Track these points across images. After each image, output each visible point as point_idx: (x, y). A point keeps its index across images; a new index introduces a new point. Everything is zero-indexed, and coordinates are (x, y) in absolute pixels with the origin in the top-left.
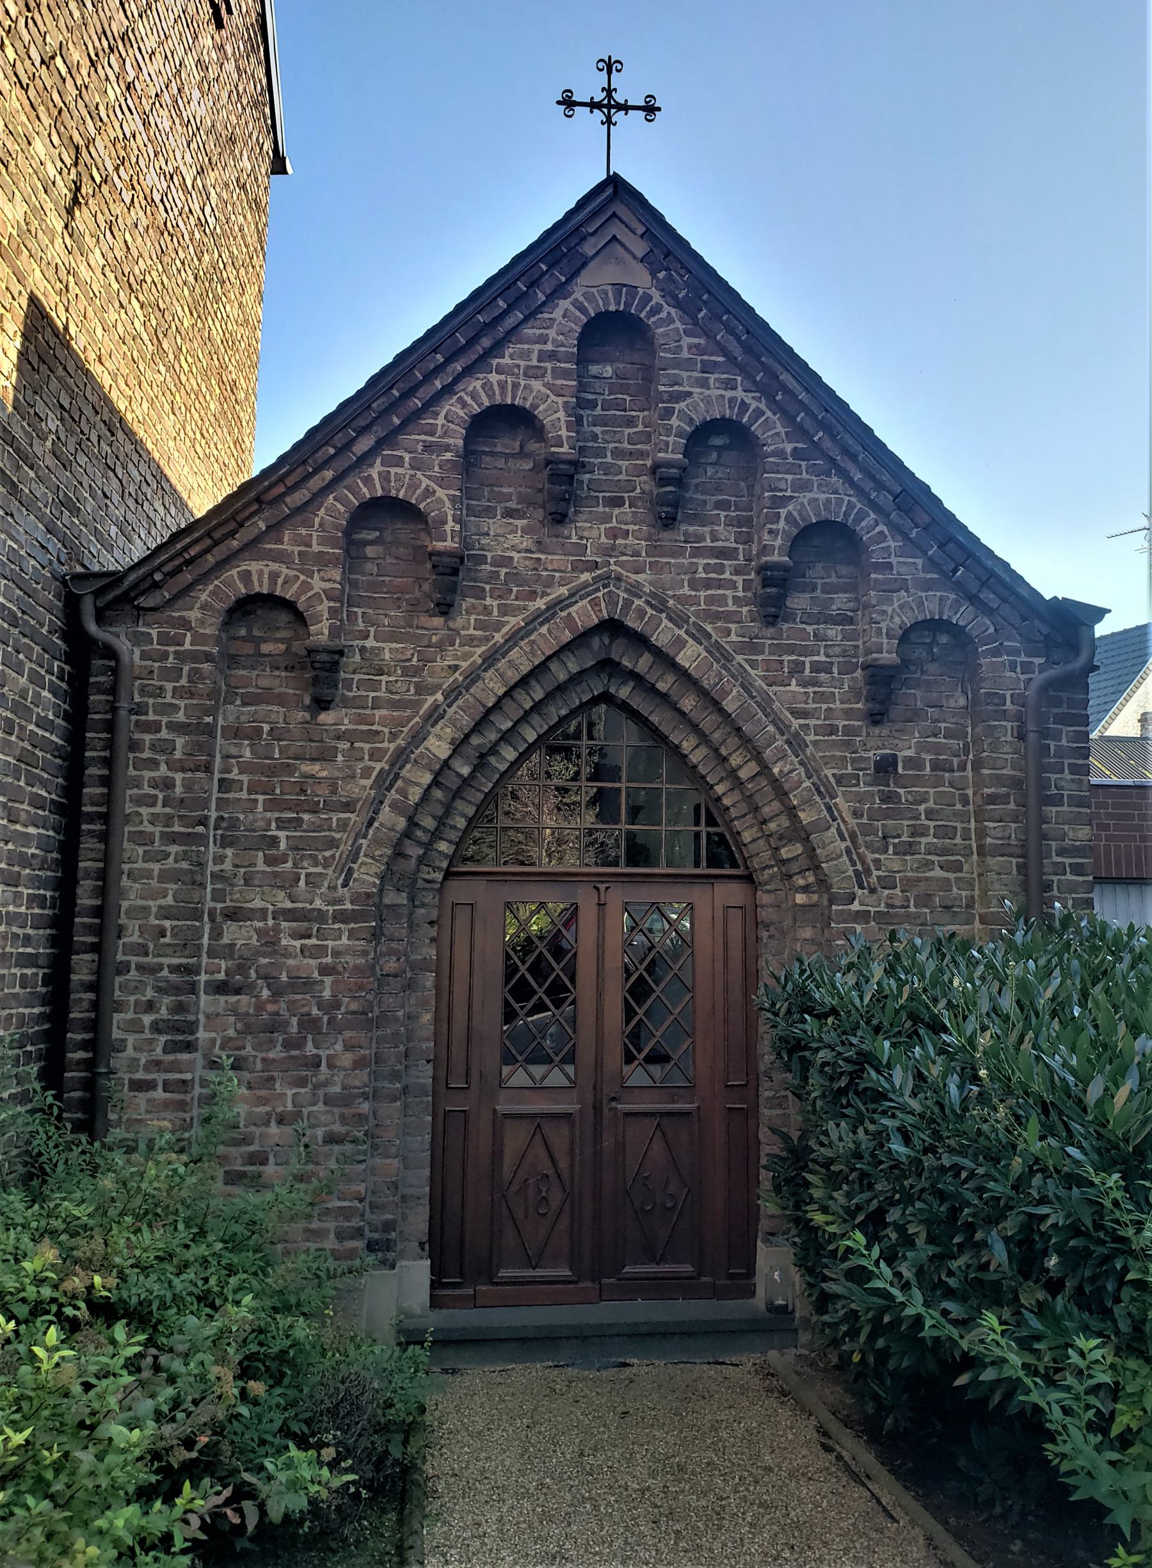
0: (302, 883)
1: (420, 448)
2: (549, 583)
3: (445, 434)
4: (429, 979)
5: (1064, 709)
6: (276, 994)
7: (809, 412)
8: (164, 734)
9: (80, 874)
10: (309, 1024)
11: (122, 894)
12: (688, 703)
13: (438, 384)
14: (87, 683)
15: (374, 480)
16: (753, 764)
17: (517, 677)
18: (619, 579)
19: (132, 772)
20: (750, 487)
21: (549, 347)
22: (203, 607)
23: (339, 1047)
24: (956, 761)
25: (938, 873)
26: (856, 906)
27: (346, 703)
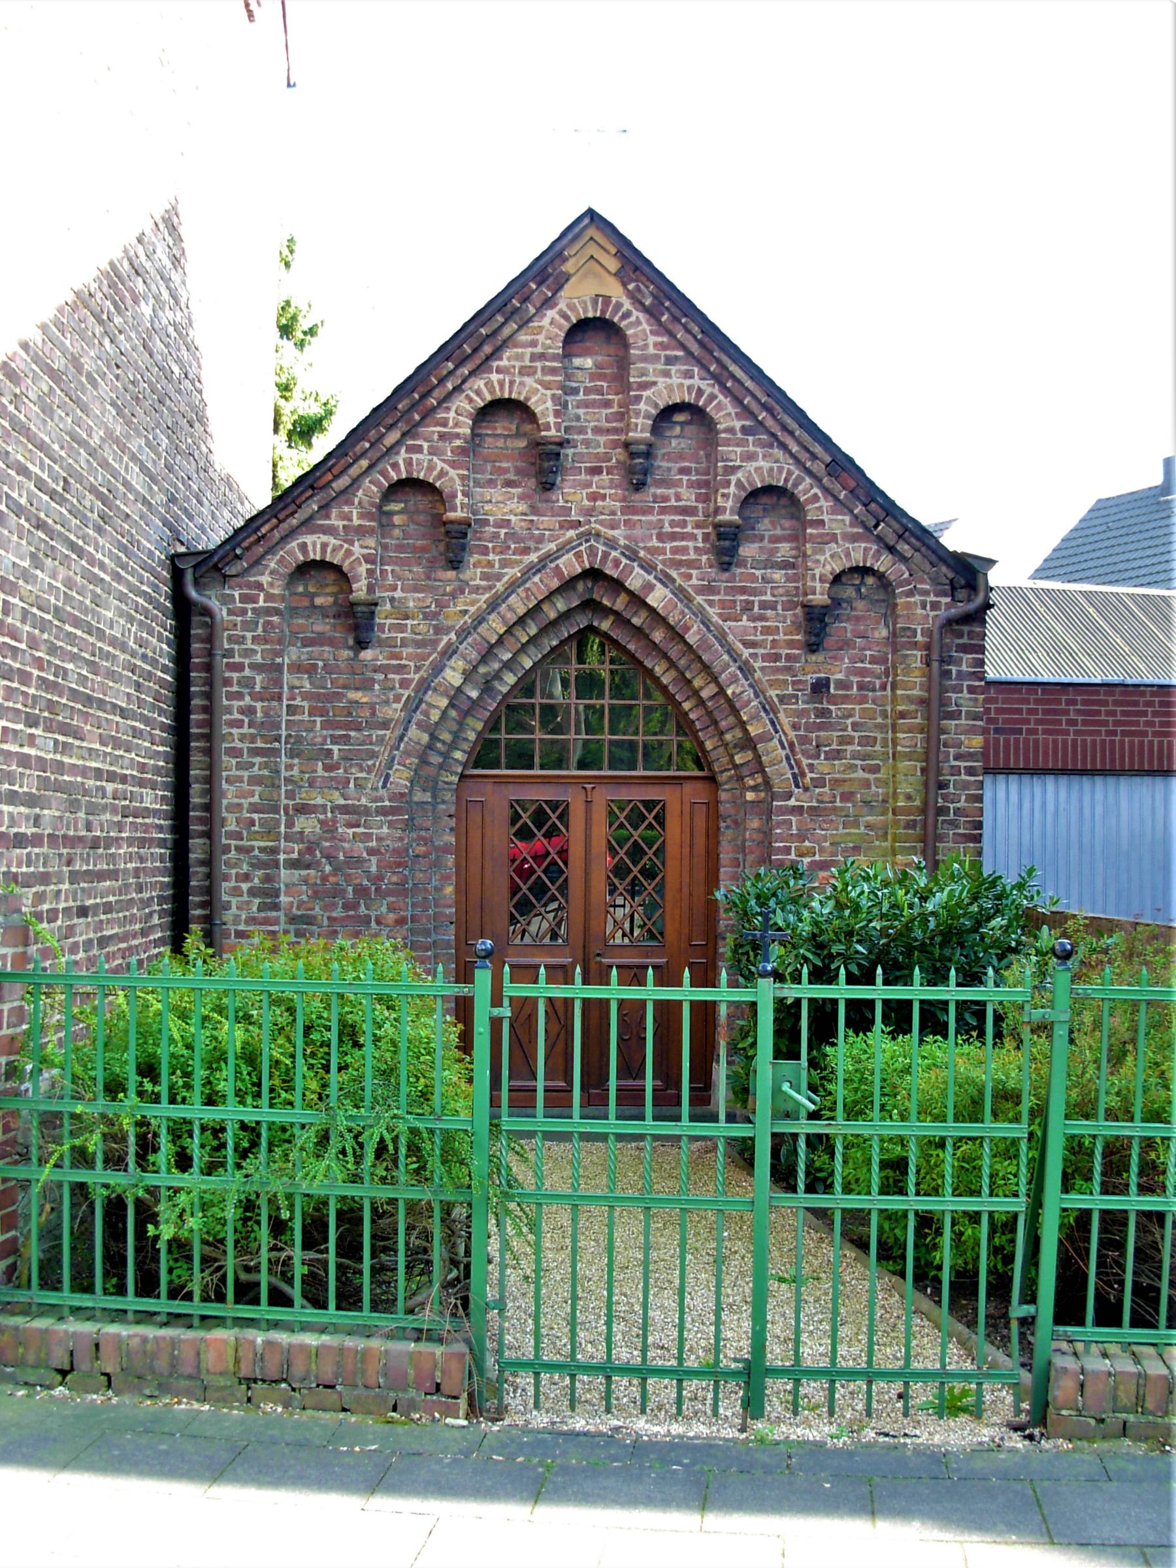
0: (352, 785)
1: (436, 437)
2: (540, 540)
3: (456, 425)
4: (451, 859)
5: (965, 640)
6: (336, 870)
7: (754, 397)
8: (247, 672)
9: (191, 780)
10: (361, 891)
11: (223, 794)
12: (658, 636)
13: (450, 386)
14: (189, 635)
15: (401, 465)
16: (712, 685)
17: (515, 619)
18: (598, 535)
19: (225, 702)
20: (708, 456)
21: (539, 349)
22: (272, 573)
23: (384, 909)
24: (878, 682)
25: (860, 774)
26: (792, 802)
27: (381, 643)
